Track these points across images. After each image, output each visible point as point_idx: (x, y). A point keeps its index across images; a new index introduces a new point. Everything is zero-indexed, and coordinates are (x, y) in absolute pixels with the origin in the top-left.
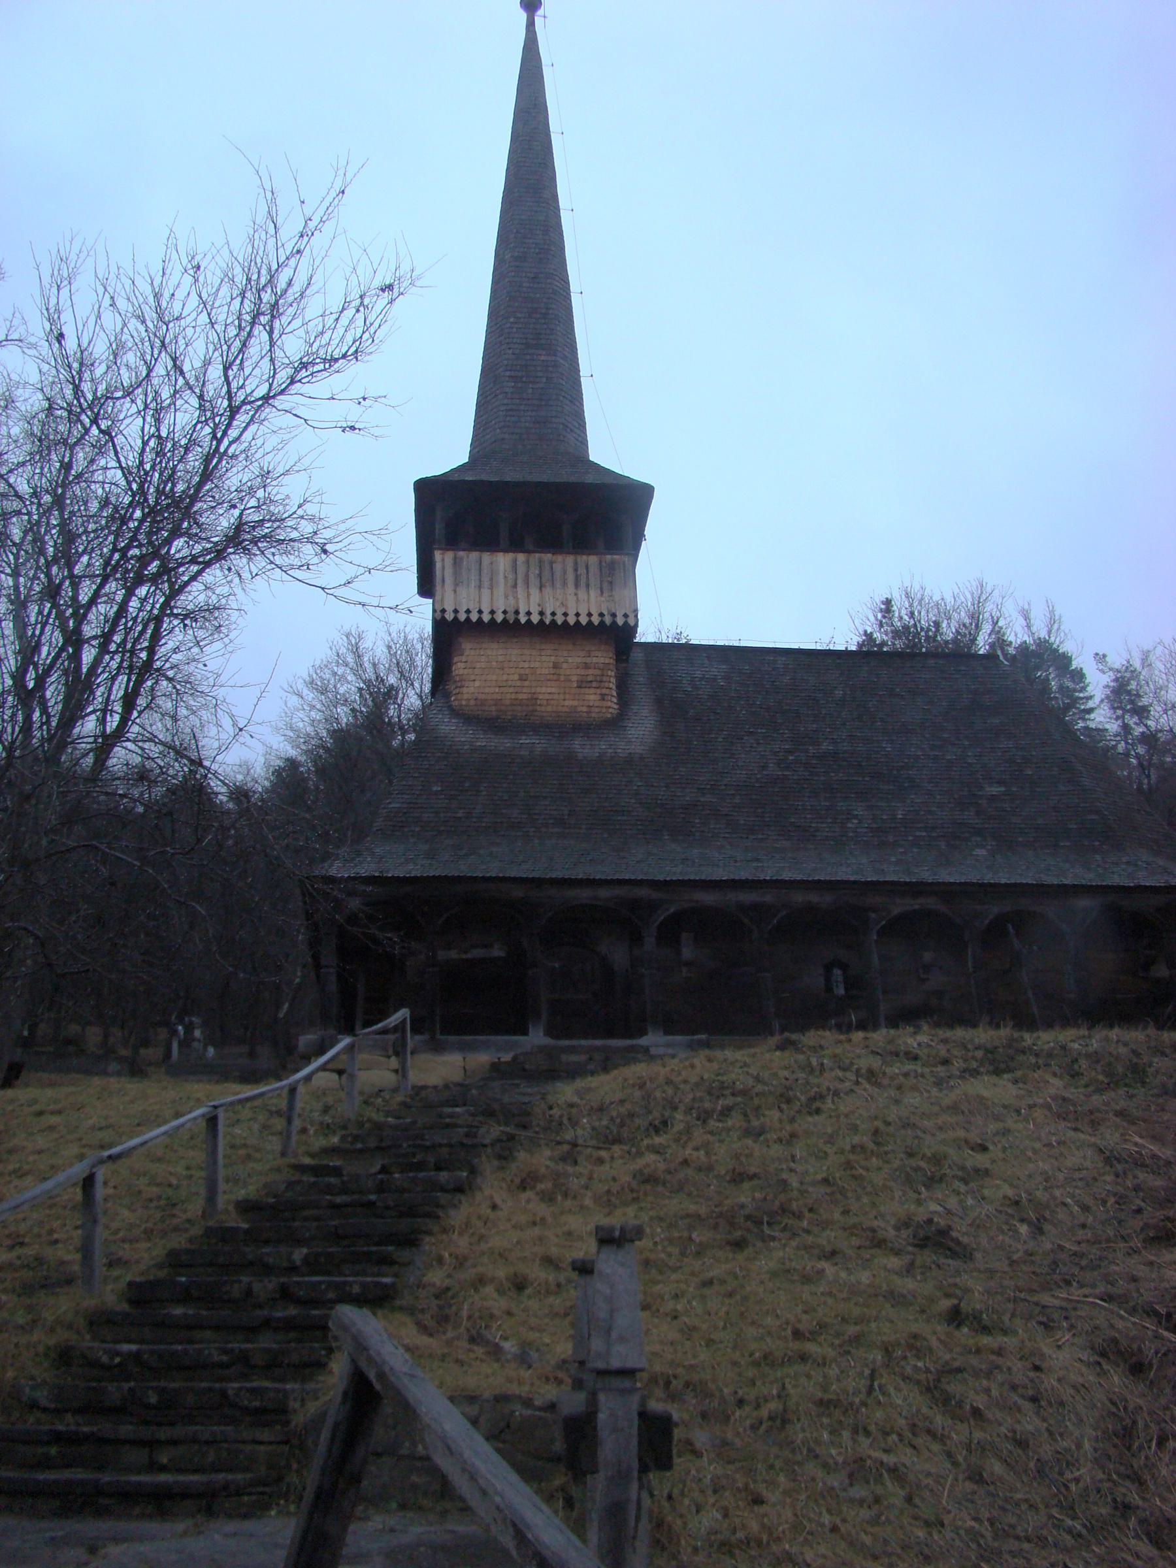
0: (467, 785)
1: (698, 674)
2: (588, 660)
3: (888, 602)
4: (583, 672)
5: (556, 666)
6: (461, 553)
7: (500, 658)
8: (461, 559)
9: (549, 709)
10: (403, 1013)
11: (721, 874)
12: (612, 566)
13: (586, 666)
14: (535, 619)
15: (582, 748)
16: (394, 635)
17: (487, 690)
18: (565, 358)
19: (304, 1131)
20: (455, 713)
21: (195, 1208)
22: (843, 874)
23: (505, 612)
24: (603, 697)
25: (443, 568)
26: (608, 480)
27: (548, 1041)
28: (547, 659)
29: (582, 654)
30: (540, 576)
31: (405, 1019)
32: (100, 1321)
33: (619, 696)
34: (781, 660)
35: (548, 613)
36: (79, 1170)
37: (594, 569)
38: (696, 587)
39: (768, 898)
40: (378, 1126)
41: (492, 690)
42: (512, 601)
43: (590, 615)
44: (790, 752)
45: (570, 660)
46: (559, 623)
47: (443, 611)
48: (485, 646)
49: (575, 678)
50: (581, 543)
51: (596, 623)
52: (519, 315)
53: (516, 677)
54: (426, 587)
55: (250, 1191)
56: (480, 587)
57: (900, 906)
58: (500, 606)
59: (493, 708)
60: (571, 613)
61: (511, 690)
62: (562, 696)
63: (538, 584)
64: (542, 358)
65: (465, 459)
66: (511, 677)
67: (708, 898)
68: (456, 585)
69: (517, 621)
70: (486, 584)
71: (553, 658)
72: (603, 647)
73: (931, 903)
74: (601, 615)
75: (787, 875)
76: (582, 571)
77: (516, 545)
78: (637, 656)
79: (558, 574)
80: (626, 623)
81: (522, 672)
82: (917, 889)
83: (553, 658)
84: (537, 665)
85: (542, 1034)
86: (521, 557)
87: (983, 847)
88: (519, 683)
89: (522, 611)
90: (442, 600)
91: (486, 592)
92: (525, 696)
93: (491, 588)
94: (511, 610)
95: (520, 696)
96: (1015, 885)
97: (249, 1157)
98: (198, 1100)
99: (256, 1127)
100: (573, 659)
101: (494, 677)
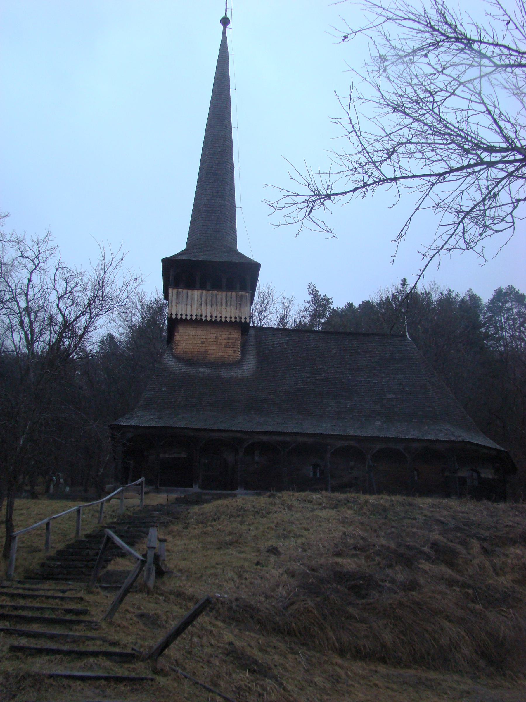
1: (276, 342)
2: (230, 336)
3: (404, 280)
5: (216, 338)
6: (180, 290)
8: (180, 293)
9: (213, 356)
10: (142, 479)
11: (271, 429)
14: (209, 319)
15: (224, 373)
19: (105, 517)
20: (174, 356)
21: (73, 536)
22: (319, 431)
23: (196, 316)
24: (235, 352)
27: (200, 490)
28: (213, 335)
29: (228, 333)
30: (212, 300)
31: (143, 481)
32: (50, 558)
35: (214, 316)
36: (46, 520)
37: (234, 299)
39: (288, 439)
40: (130, 517)
41: (190, 347)
42: (199, 311)
44: (308, 377)
45: (222, 336)
46: (218, 321)
47: (171, 314)
48: (188, 329)
49: (223, 344)
50: (230, 288)
51: (233, 321)
52: (210, 181)
53: (200, 342)
55: (89, 532)
56: (187, 305)
57: (341, 444)
58: (195, 313)
60: (224, 316)
61: (198, 348)
64: (219, 201)
65: (184, 247)
67: (265, 438)
68: (177, 303)
69: (201, 319)
70: (189, 304)
72: (236, 331)
73: (352, 443)
74: (236, 318)
76: (229, 299)
77: (202, 287)
79: (219, 300)
80: (245, 322)
81: (203, 340)
82: (347, 438)
84: (209, 337)
85: (197, 487)
86: (204, 292)
87: (380, 421)
89: (204, 315)
90: (171, 310)
91: (189, 307)
93: (191, 305)
94: (199, 315)
95: (201, 350)
97: (88, 524)
98: (70, 507)
99: (90, 515)
100: (223, 335)
101: (191, 342)
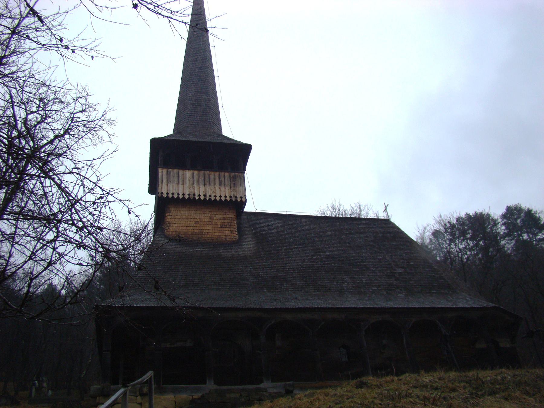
0: (173, 267)
2: (225, 216)
4: (223, 221)
5: (211, 218)
6: (170, 170)
7: (186, 214)
8: (170, 172)
10: (150, 374)
12: (235, 177)
13: (224, 219)
14: (202, 198)
16: (133, 223)
17: (181, 228)
18: (213, 98)
20: (166, 237)
23: (189, 195)
25: (162, 175)
26: (232, 142)
27: (216, 387)
30: (204, 180)
31: (151, 377)
33: (238, 232)
34: (303, 220)
35: (208, 195)
38: (267, 191)
41: (183, 228)
42: (192, 190)
43: (226, 197)
44: (313, 255)
45: (217, 216)
46: (213, 199)
50: (221, 168)
53: (194, 223)
54: (153, 189)
56: (178, 184)
58: (187, 192)
59: (184, 236)
60: (218, 196)
62: (214, 231)
63: (203, 183)
65: (171, 132)
66: (191, 223)
69: (194, 198)
70: (181, 183)
71: (210, 215)
75: (324, 306)
77: (193, 167)
78: (244, 216)
79: (212, 180)
80: (241, 201)
81: (196, 220)
83: (210, 215)
84: (203, 218)
85: (213, 383)
86: (196, 172)
88: (195, 225)
89: (197, 194)
90: (162, 188)
91: (181, 186)
92: (197, 231)
93: (183, 184)
95: (196, 231)
96: (422, 308)
100: (218, 216)
101: (184, 222)
